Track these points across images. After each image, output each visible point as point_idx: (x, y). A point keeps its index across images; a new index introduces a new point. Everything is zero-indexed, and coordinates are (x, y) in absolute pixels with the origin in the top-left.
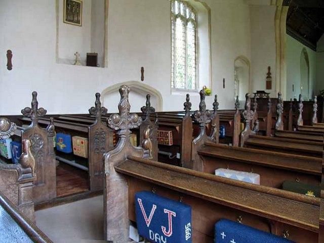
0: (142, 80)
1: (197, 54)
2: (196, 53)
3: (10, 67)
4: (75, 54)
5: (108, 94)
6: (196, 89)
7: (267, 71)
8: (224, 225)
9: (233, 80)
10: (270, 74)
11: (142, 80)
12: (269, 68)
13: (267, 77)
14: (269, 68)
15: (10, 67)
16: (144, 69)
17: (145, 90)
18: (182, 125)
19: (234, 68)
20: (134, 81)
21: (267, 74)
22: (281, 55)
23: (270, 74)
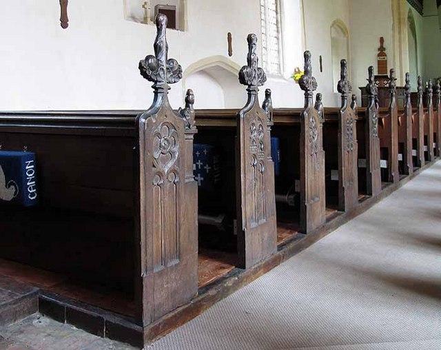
0: (230, 55)
1: (279, 15)
2: (277, 13)
3: (64, 23)
4: (143, 6)
5: (200, 74)
6: (280, 73)
7: (378, 45)
8: (216, 289)
9: (330, 56)
10: (384, 49)
11: (230, 55)
12: (382, 40)
13: (379, 55)
14: (382, 40)
15: (64, 23)
16: (232, 37)
17: (229, 69)
18: (390, 116)
19: (330, 40)
20: (221, 56)
21: (379, 50)
22: (399, 19)
23: (384, 49)
